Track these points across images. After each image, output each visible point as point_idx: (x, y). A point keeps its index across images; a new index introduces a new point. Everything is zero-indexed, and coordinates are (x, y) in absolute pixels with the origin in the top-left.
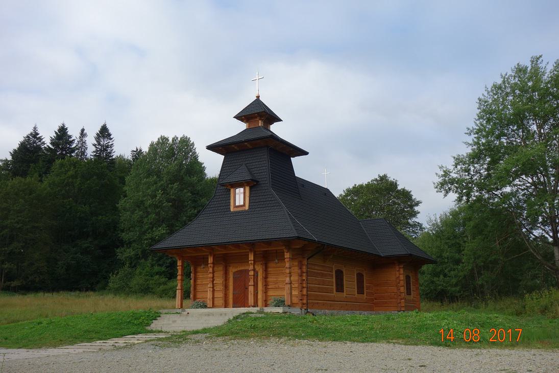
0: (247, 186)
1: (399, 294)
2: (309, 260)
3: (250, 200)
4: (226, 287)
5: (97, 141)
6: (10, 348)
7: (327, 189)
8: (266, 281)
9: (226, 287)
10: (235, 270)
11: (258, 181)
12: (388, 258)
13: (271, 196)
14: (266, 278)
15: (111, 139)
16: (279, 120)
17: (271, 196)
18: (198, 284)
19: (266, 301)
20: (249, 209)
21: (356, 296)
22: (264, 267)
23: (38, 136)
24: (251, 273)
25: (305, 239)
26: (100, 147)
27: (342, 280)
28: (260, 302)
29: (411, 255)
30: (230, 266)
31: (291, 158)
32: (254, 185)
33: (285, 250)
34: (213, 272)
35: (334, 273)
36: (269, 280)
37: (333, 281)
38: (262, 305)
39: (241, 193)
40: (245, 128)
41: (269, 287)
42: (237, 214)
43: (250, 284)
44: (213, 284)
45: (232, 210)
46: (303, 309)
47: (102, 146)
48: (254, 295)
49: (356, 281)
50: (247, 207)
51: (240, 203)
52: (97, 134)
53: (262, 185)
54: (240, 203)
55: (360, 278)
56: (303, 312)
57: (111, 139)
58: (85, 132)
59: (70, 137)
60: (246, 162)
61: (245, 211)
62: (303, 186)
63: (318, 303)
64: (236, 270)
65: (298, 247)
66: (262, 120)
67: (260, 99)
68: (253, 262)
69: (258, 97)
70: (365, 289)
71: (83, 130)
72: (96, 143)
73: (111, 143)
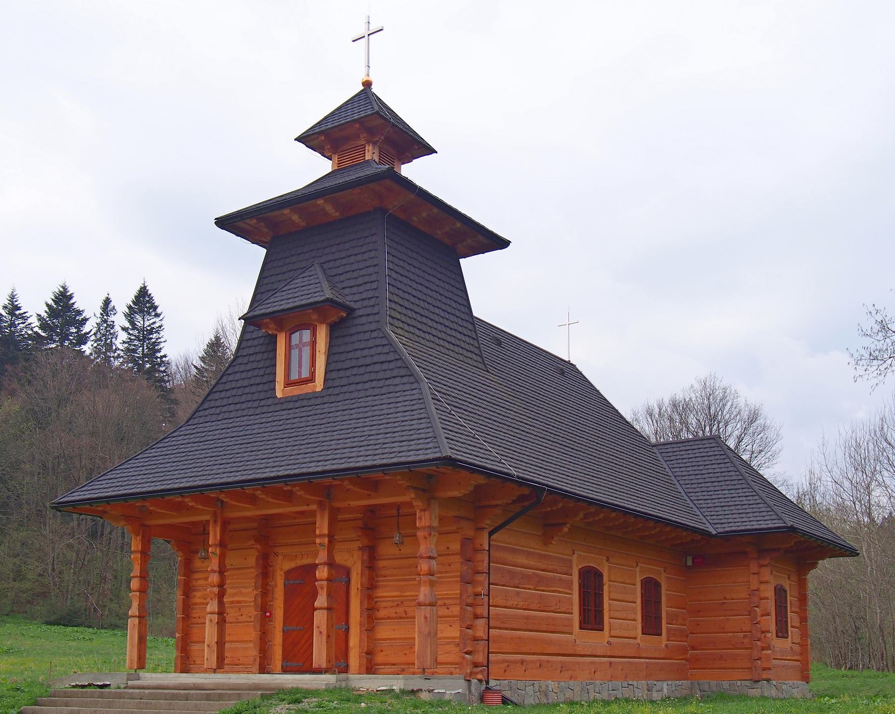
0: (321, 323)
1: (759, 635)
2: (493, 537)
3: (328, 364)
4: (265, 612)
5: (129, 321)
6: (580, 578)
7: (569, 362)
8: (370, 598)
9: (265, 612)
10: (289, 565)
11: (353, 310)
12: (728, 537)
13: (386, 349)
14: (370, 587)
15: (157, 315)
16: (428, 150)
17: (386, 349)
18: (196, 604)
19: (370, 653)
20: (326, 388)
21: (638, 641)
22: (366, 557)
23: (18, 312)
24: (322, 573)
25: (474, 469)
26: (136, 332)
27: (599, 596)
28: (354, 659)
29: (792, 529)
30: (276, 555)
31: (461, 261)
32: (342, 320)
33: (417, 503)
34: (221, 572)
35: (575, 578)
36: (380, 593)
37: (571, 599)
38: (360, 667)
39: (304, 345)
40: (330, 170)
41: (382, 613)
42: (291, 405)
43: (317, 604)
44: (221, 603)
45: (279, 395)
46: (474, 681)
47: (142, 329)
48: (328, 636)
49: (639, 601)
50: (319, 384)
51: (300, 373)
52: (130, 307)
53: (364, 320)
54: (300, 373)
55: (651, 589)
56: (473, 689)
57: (157, 315)
58: (112, 304)
59: (79, 313)
60: (323, 259)
61: (315, 395)
62: (499, 343)
63: (522, 662)
64: (292, 565)
65: (456, 493)
66: (374, 143)
67: (375, 89)
68: (326, 540)
69: (367, 84)
70: (664, 622)
71: (107, 302)
72: (127, 325)
73: (157, 325)
